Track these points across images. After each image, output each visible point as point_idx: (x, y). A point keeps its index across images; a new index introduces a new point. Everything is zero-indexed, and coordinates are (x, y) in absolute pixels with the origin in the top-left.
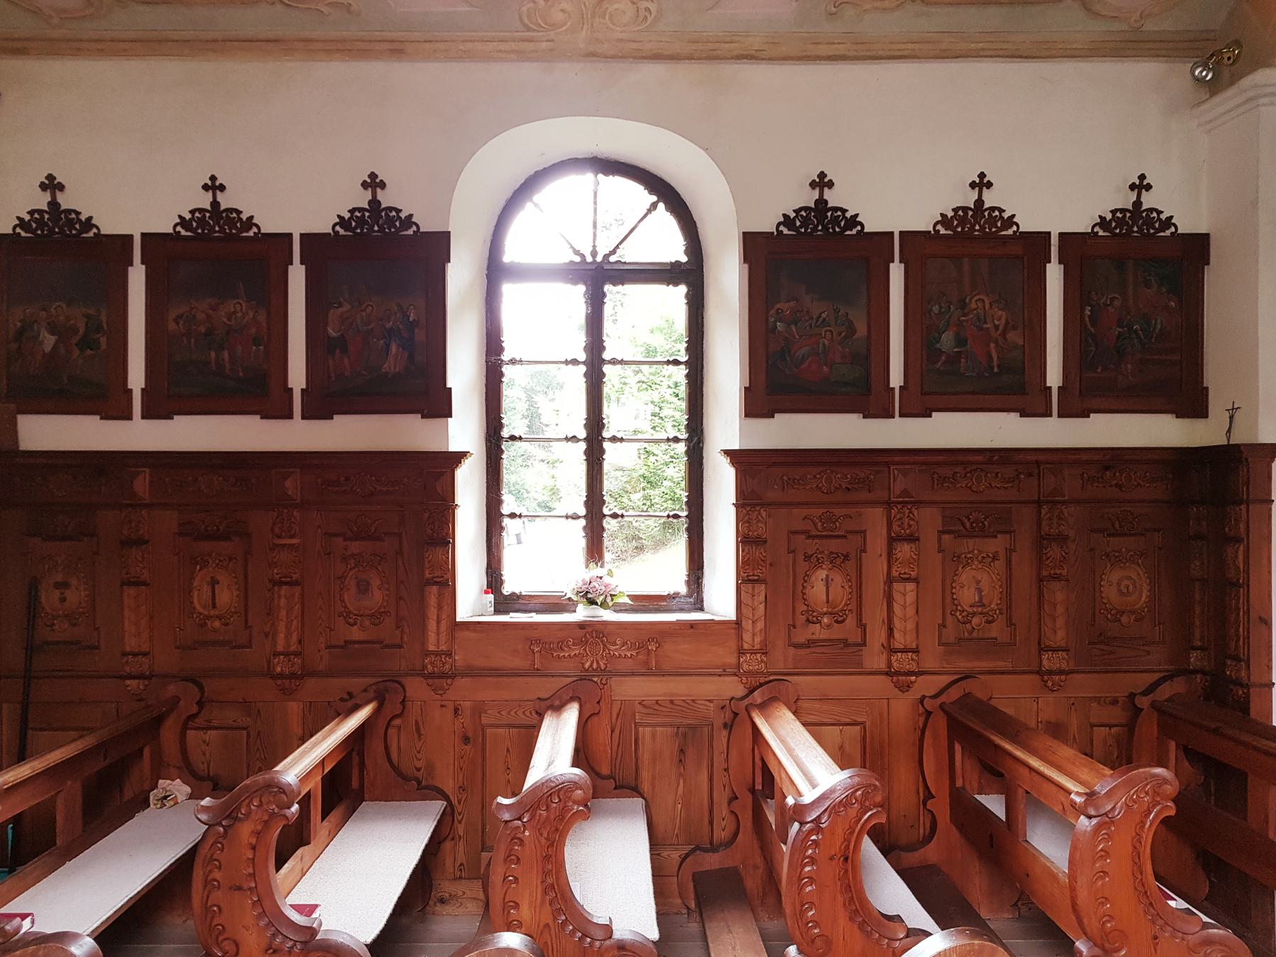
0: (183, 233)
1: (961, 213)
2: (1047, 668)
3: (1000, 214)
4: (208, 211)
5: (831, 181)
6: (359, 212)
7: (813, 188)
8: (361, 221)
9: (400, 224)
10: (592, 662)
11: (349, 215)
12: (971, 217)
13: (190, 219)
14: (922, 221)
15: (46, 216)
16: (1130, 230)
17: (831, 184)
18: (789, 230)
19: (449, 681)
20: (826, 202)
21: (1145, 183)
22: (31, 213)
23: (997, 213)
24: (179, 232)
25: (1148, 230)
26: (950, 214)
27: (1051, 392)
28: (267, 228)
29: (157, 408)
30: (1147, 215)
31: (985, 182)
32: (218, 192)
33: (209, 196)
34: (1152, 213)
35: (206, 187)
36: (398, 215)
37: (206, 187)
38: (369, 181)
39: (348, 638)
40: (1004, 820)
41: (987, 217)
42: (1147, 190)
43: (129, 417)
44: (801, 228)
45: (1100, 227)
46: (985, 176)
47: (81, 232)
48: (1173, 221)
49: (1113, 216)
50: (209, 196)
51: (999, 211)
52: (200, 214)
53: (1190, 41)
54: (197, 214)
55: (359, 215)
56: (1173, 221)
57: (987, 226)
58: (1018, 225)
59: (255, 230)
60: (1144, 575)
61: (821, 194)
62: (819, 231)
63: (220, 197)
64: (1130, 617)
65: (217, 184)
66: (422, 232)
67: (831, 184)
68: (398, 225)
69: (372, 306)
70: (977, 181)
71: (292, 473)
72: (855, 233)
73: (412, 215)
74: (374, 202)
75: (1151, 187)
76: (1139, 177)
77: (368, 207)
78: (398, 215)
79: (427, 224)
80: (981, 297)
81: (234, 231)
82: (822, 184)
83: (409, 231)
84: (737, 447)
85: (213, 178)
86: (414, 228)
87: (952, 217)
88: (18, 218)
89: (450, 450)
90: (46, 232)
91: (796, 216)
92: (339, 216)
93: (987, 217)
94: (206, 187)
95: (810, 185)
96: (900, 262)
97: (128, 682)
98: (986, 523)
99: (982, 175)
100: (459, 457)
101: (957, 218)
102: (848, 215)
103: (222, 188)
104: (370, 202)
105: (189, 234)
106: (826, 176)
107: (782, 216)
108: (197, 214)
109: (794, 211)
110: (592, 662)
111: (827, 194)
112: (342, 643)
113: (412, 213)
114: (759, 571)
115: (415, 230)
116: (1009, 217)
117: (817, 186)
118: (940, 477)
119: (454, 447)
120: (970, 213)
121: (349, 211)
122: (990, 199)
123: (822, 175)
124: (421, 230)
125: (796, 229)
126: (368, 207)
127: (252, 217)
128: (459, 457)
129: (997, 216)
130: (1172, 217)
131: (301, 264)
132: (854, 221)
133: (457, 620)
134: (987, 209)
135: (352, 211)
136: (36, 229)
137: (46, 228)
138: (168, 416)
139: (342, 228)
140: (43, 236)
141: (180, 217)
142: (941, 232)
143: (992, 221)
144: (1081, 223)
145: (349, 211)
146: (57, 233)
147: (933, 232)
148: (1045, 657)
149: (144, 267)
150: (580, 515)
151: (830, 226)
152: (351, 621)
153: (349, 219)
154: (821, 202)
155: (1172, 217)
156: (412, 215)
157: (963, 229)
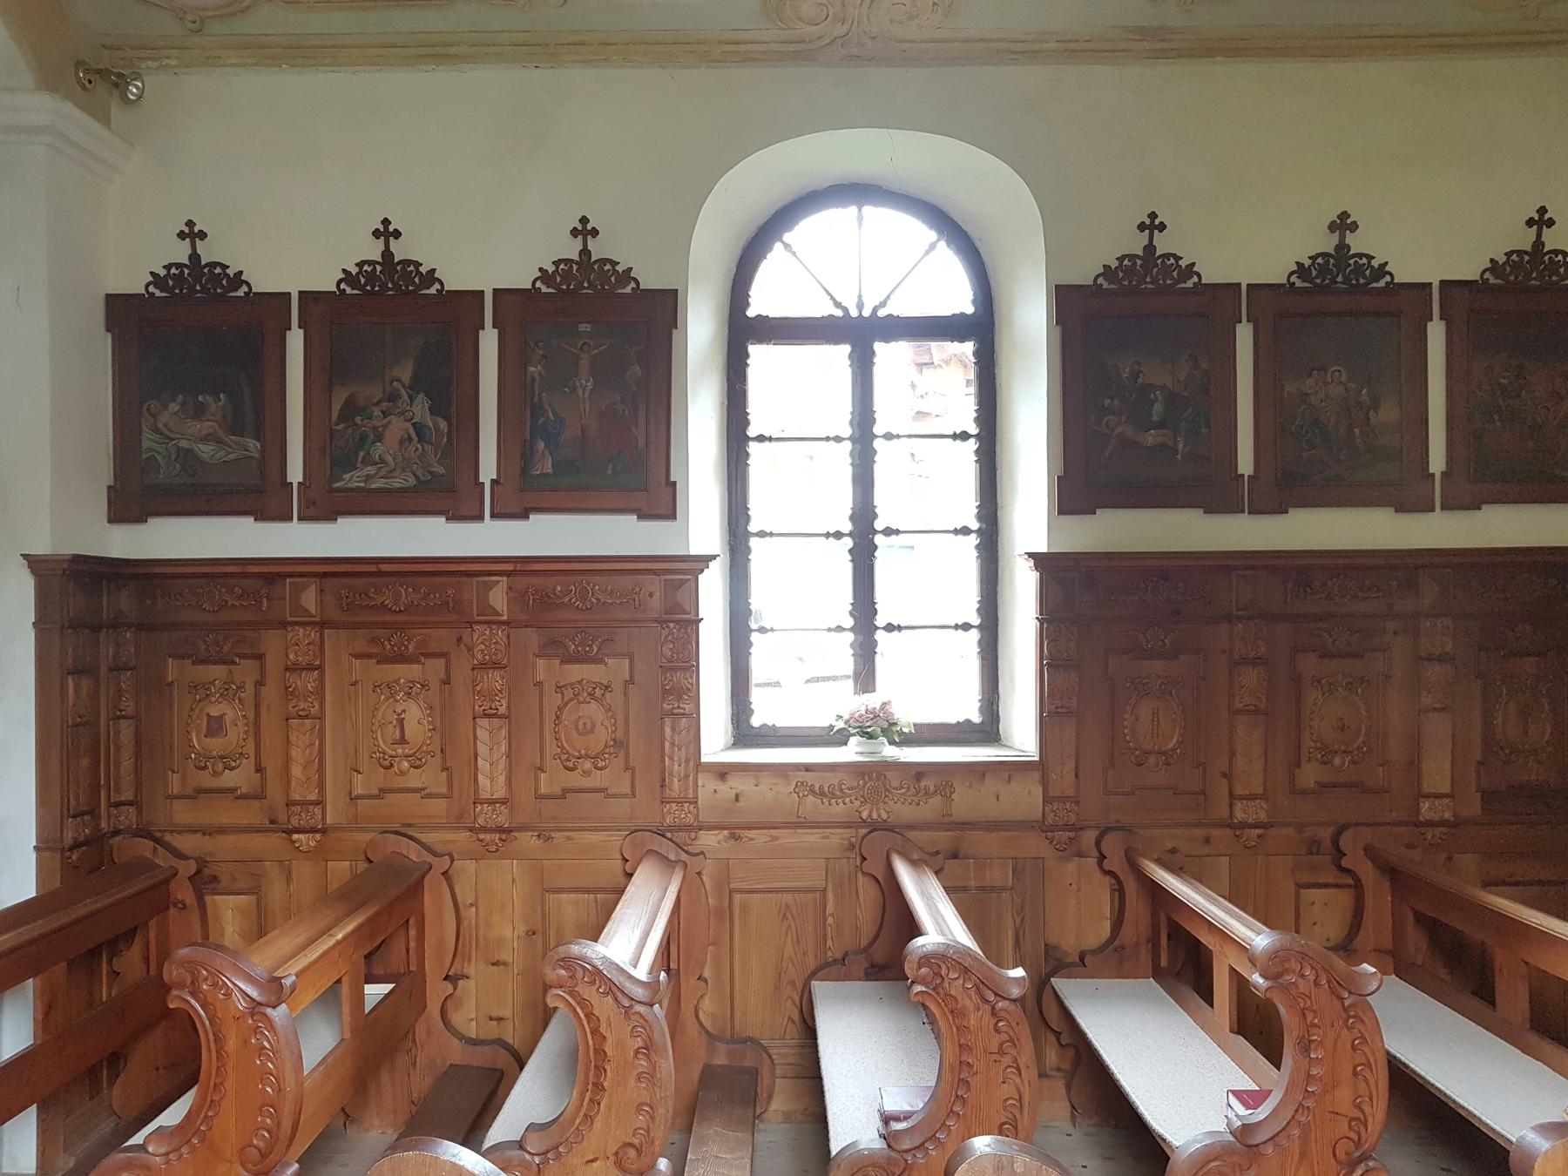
0: (544, 289)
1: (1514, 257)
2: (1239, 819)
3: (1177, 262)
4: (185, 266)
5: (186, 224)
6: (369, 266)
7: (1332, 232)
8: (371, 277)
9: (616, 279)
10: (871, 811)
11: (357, 269)
12: (380, 272)
13: (165, 275)
14: (1275, 271)
15: (379, 268)
16: (192, 290)
17: (1354, 227)
18: (161, 291)
19: (693, 835)
20: (1349, 247)
21: (196, 231)
22: (168, 267)
23: (1172, 261)
24: (344, 290)
25: (1357, 280)
26: (551, 269)
27: (1434, 479)
28: (258, 287)
29: (514, 508)
30: (209, 270)
31: (1546, 218)
32: (589, 237)
33: (577, 244)
34: (1169, 260)
35: (181, 235)
36: (614, 269)
37: (181, 235)
38: (1349, 221)
39: (568, 785)
40: (367, 1010)
41: (1547, 262)
42: (1549, 227)
43: (291, 519)
44: (1124, 280)
45: (1104, 279)
46: (1157, 216)
47: (419, 287)
48: (1195, 269)
49: (1121, 263)
50: (577, 244)
51: (1175, 259)
52: (177, 269)
53: (1065, 41)
54: (173, 270)
55: (369, 269)
56: (1195, 269)
57: (1160, 277)
58: (1199, 276)
59: (1100, 281)
60: (1501, 702)
61: (1342, 238)
62: (1533, 279)
63: (394, 245)
64: (1343, 758)
65: (589, 228)
66: (1205, 284)
67: (1354, 227)
68: (613, 281)
69: (1339, 371)
70: (1148, 222)
71: (499, 582)
72: (1383, 285)
73: (632, 268)
74: (1342, 247)
75: (1554, 223)
76: (383, 222)
77: (188, 263)
78: (614, 269)
79: (650, 279)
80: (1341, 369)
81: (219, 291)
82: (584, 232)
83: (431, 289)
84: (1045, 550)
85: (190, 224)
86: (633, 285)
87: (553, 272)
88: (541, 269)
89: (692, 553)
90: (377, 289)
91: (360, 272)
92: (152, 273)
93: (1547, 262)
94: (376, 234)
95: (572, 232)
96: (1248, 321)
97: (295, 836)
98: (1166, 641)
99: (1153, 216)
100: (705, 560)
101: (1316, 266)
102: (620, 268)
103: (202, 235)
104: (190, 257)
105: (1499, 281)
106: (1349, 216)
107: (1295, 265)
108: (173, 270)
109: (1310, 258)
110: (871, 811)
111: (1350, 238)
112: (376, 792)
113: (240, 269)
114: (497, 703)
115: (439, 288)
116: (1187, 266)
117: (1338, 229)
118: (536, 591)
119: (696, 549)
120: (1139, 262)
121: (357, 265)
122: (1163, 244)
123: (1344, 215)
124: (254, 290)
125: (362, 288)
126: (188, 263)
127: (433, 271)
128: (705, 560)
129: (1560, 261)
130: (1193, 264)
131: (494, 327)
132: (238, 280)
133: (704, 759)
134: (1159, 257)
135: (360, 265)
136: (174, 287)
137: (1329, 277)
138: (141, 519)
139: (157, 288)
140: (372, 293)
141: (541, 269)
142: (1491, 282)
143: (1167, 271)
144: (1468, 268)
145: (357, 265)
146: (391, 289)
147: (338, 293)
148: (1238, 805)
149: (496, 331)
150: (757, 633)
151: (1547, 273)
152: (570, 764)
153: (357, 274)
154: (1342, 247)
155: (1193, 264)
156: (632, 268)
157: (1130, 282)
